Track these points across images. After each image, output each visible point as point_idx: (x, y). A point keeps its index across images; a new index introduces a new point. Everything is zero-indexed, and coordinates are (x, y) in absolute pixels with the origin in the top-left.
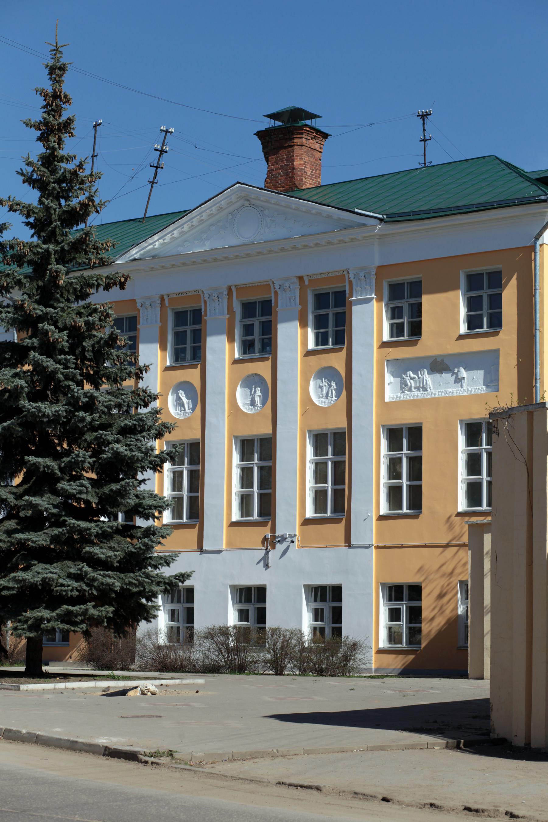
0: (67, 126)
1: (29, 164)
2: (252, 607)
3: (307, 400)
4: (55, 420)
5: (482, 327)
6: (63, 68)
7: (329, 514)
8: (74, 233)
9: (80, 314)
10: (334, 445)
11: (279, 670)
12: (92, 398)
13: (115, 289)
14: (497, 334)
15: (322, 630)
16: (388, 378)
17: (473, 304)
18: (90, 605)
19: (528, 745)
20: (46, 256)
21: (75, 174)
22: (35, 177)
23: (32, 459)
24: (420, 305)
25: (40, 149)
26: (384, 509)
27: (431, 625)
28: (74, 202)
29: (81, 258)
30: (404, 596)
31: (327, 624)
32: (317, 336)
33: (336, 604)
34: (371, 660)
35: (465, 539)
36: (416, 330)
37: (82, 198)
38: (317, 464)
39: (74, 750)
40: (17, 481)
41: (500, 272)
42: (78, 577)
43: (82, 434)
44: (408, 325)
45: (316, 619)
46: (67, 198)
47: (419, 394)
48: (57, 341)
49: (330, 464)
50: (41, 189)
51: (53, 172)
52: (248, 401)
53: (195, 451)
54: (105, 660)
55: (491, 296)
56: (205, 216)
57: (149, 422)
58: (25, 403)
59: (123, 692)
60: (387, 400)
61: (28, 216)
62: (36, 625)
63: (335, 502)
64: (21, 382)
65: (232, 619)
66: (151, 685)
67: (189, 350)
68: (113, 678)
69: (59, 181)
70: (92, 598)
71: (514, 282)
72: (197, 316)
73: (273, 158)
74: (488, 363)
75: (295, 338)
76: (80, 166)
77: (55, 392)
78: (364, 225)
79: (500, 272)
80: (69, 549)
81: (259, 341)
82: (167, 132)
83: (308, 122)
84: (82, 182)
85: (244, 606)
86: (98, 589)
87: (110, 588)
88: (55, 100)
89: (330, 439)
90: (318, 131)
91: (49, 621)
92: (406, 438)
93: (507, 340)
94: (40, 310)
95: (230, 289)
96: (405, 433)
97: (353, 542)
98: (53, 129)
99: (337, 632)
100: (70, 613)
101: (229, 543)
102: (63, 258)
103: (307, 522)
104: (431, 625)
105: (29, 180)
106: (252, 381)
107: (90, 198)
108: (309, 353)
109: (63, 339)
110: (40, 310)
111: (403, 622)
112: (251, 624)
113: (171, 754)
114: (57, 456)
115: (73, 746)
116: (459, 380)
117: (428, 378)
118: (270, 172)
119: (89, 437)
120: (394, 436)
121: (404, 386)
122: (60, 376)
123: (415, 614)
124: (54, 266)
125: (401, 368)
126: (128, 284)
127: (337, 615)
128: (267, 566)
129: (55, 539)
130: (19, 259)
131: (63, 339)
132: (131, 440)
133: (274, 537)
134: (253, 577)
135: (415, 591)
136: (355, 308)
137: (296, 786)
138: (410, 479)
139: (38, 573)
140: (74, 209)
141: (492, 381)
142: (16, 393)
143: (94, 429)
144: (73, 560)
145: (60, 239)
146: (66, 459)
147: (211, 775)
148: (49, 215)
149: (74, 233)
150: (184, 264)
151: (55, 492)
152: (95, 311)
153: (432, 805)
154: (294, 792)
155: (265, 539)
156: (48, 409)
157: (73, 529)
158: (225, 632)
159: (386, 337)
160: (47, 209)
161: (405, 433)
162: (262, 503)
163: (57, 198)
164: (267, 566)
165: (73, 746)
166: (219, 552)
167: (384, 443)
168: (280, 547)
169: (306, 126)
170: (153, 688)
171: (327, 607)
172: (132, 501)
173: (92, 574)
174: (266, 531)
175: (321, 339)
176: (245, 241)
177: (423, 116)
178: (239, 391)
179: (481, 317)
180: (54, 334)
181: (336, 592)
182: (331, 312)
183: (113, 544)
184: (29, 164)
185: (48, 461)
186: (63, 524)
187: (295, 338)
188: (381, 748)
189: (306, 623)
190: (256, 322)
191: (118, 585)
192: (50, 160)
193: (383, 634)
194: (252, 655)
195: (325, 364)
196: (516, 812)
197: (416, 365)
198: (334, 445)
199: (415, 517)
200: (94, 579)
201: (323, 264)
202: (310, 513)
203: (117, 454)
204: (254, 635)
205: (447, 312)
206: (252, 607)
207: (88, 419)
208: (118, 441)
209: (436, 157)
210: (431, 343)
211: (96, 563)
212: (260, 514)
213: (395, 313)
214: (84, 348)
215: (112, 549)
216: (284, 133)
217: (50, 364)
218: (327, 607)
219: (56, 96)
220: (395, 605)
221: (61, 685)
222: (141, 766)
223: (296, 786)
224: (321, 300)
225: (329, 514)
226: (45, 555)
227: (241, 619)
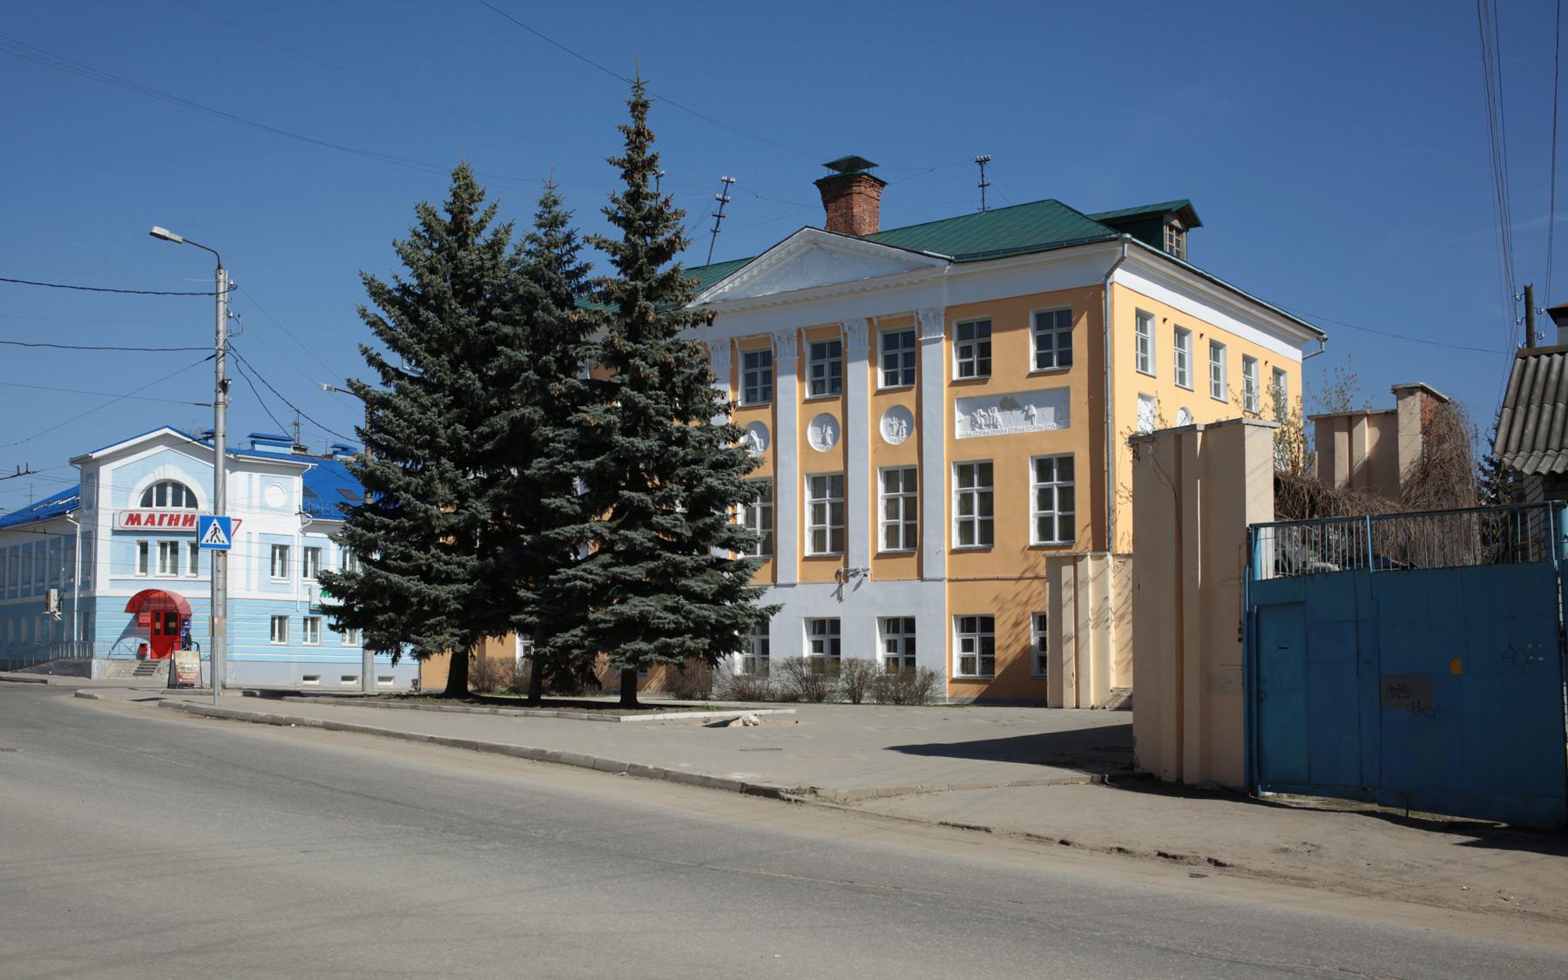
0: (650, 163)
1: (615, 201)
2: (826, 639)
3: (878, 438)
4: (648, 456)
5: (1051, 364)
6: (645, 105)
7: (901, 548)
8: (663, 269)
9: (669, 350)
10: (905, 482)
11: (856, 698)
12: (685, 433)
13: (703, 326)
14: (1067, 371)
15: (896, 660)
16: (958, 415)
17: (1042, 343)
18: (687, 636)
19: (1180, 780)
20: (633, 293)
21: (661, 211)
22: (620, 214)
23: (626, 493)
24: (989, 344)
25: (623, 187)
26: (956, 543)
27: (1005, 654)
28: (660, 239)
29: (667, 295)
30: (978, 627)
31: (900, 655)
32: (886, 375)
33: (909, 636)
34: (945, 689)
35: (1044, 573)
36: (986, 369)
37: (669, 234)
38: (815, 506)
39: (708, 786)
40: (607, 516)
41: (1069, 311)
42: (674, 610)
43: (674, 468)
44: (977, 362)
45: (889, 650)
46: (653, 236)
47: (989, 432)
48: (648, 377)
49: (828, 507)
50: (625, 227)
51: (639, 209)
52: (819, 439)
53: (767, 491)
54: (686, 691)
55: (1060, 335)
56: (774, 260)
57: (740, 457)
58: (618, 438)
59: (725, 724)
61: (614, 254)
62: (635, 657)
63: (908, 536)
64: (614, 418)
65: (807, 651)
66: (750, 715)
67: (761, 390)
68: (708, 708)
69: (644, 219)
70: (688, 630)
71: (1084, 320)
72: (767, 358)
73: (832, 206)
74: (1059, 401)
75: (865, 377)
76: (666, 202)
77: (645, 429)
79: (1069, 311)
80: (663, 582)
81: (829, 377)
84: (668, 220)
85: (818, 638)
86: (694, 621)
87: (706, 620)
88: (638, 138)
89: (901, 476)
90: (875, 179)
91: (646, 653)
92: (977, 474)
93: (1077, 378)
94: (629, 346)
95: (799, 331)
96: (1055, 463)
97: (926, 575)
98: (636, 167)
99: (911, 662)
100: (667, 645)
101: (802, 577)
102: (651, 295)
103: (879, 556)
104: (1005, 654)
105: (614, 218)
106: (823, 420)
107: (677, 235)
108: (879, 393)
109: (654, 375)
110: (629, 346)
111: (976, 653)
112: (825, 654)
113: (814, 791)
114: (648, 491)
115: (705, 783)
116: (1029, 417)
117: (998, 415)
118: (829, 220)
119: (681, 471)
120: (965, 472)
121: (974, 423)
122: (652, 411)
123: (988, 646)
124: (642, 302)
125: (970, 405)
126: (715, 322)
127: (910, 646)
128: (840, 599)
129: (650, 573)
130: (606, 297)
131: (654, 375)
132: (723, 474)
133: (847, 571)
134: (827, 611)
135: (988, 623)
136: (924, 348)
137: (962, 827)
138: (833, 522)
139: (635, 606)
140: (660, 247)
141: (1063, 418)
142: (608, 429)
143: (686, 463)
144: (669, 593)
145: (646, 276)
146: (659, 494)
147: (864, 814)
148: (636, 253)
149: (663, 269)
150: (754, 308)
151: (651, 526)
152: (684, 347)
153: (1120, 850)
154: (966, 833)
155: (838, 573)
156: (640, 443)
157: (668, 562)
158: (800, 662)
159: (956, 376)
160: (634, 245)
161: (1055, 463)
162: (834, 538)
163: (643, 235)
164: (840, 599)
165: (705, 783)
166: (793, 585)
167: (955, 479)
168: (853, 581)
170: (755, 719)
171: (900, 638)
172: (725, 535)
173: (688, 606)
174: (839, 565)
175: (891, 379)
176: (814, 284)
177: (981, 162)
178: (810, 430)
179: (1051, 355)
180: (646, 370)
181: (910, 624)
182: (900, 353)
183: (706, 577)
184: (615, 201)
185: (642, 496)
186: (659, 557)
187: (865, 377)
188: (1026, 784)
189: (880, 653)
190: (826, 363)
191: (714, 616)
192: (635, 197)
193: (957, 664)
194: (828, 685)
195: (895, 403)
196: (1222, 860)
197: (986, 403)
198: (905, 482)
199: (988, 550)
200: (690, 612)
201: (891, 306)
202: (882, 548)
203: (710, 488)
204: (828, 667)
205: (1016, 351)
206: (826, 639)
207: (681, 453)
208: (710, 475)
209: (996, 201)
210: (1003, 378)
211: (698, 598)
212: (833, 549)
213: (964, 352)
214: (674, 385)
215: (706, 582)
216: (842, 183)
217: (641, 399)
218: (900, 638)
219: (639, 133)
220: (968, 636)
221: (660, 716)
222: (783, 804)
223: (962, 827)
224: (890, 341)
225: (901, 548)
226: (639, 588)
227: (815, 650)
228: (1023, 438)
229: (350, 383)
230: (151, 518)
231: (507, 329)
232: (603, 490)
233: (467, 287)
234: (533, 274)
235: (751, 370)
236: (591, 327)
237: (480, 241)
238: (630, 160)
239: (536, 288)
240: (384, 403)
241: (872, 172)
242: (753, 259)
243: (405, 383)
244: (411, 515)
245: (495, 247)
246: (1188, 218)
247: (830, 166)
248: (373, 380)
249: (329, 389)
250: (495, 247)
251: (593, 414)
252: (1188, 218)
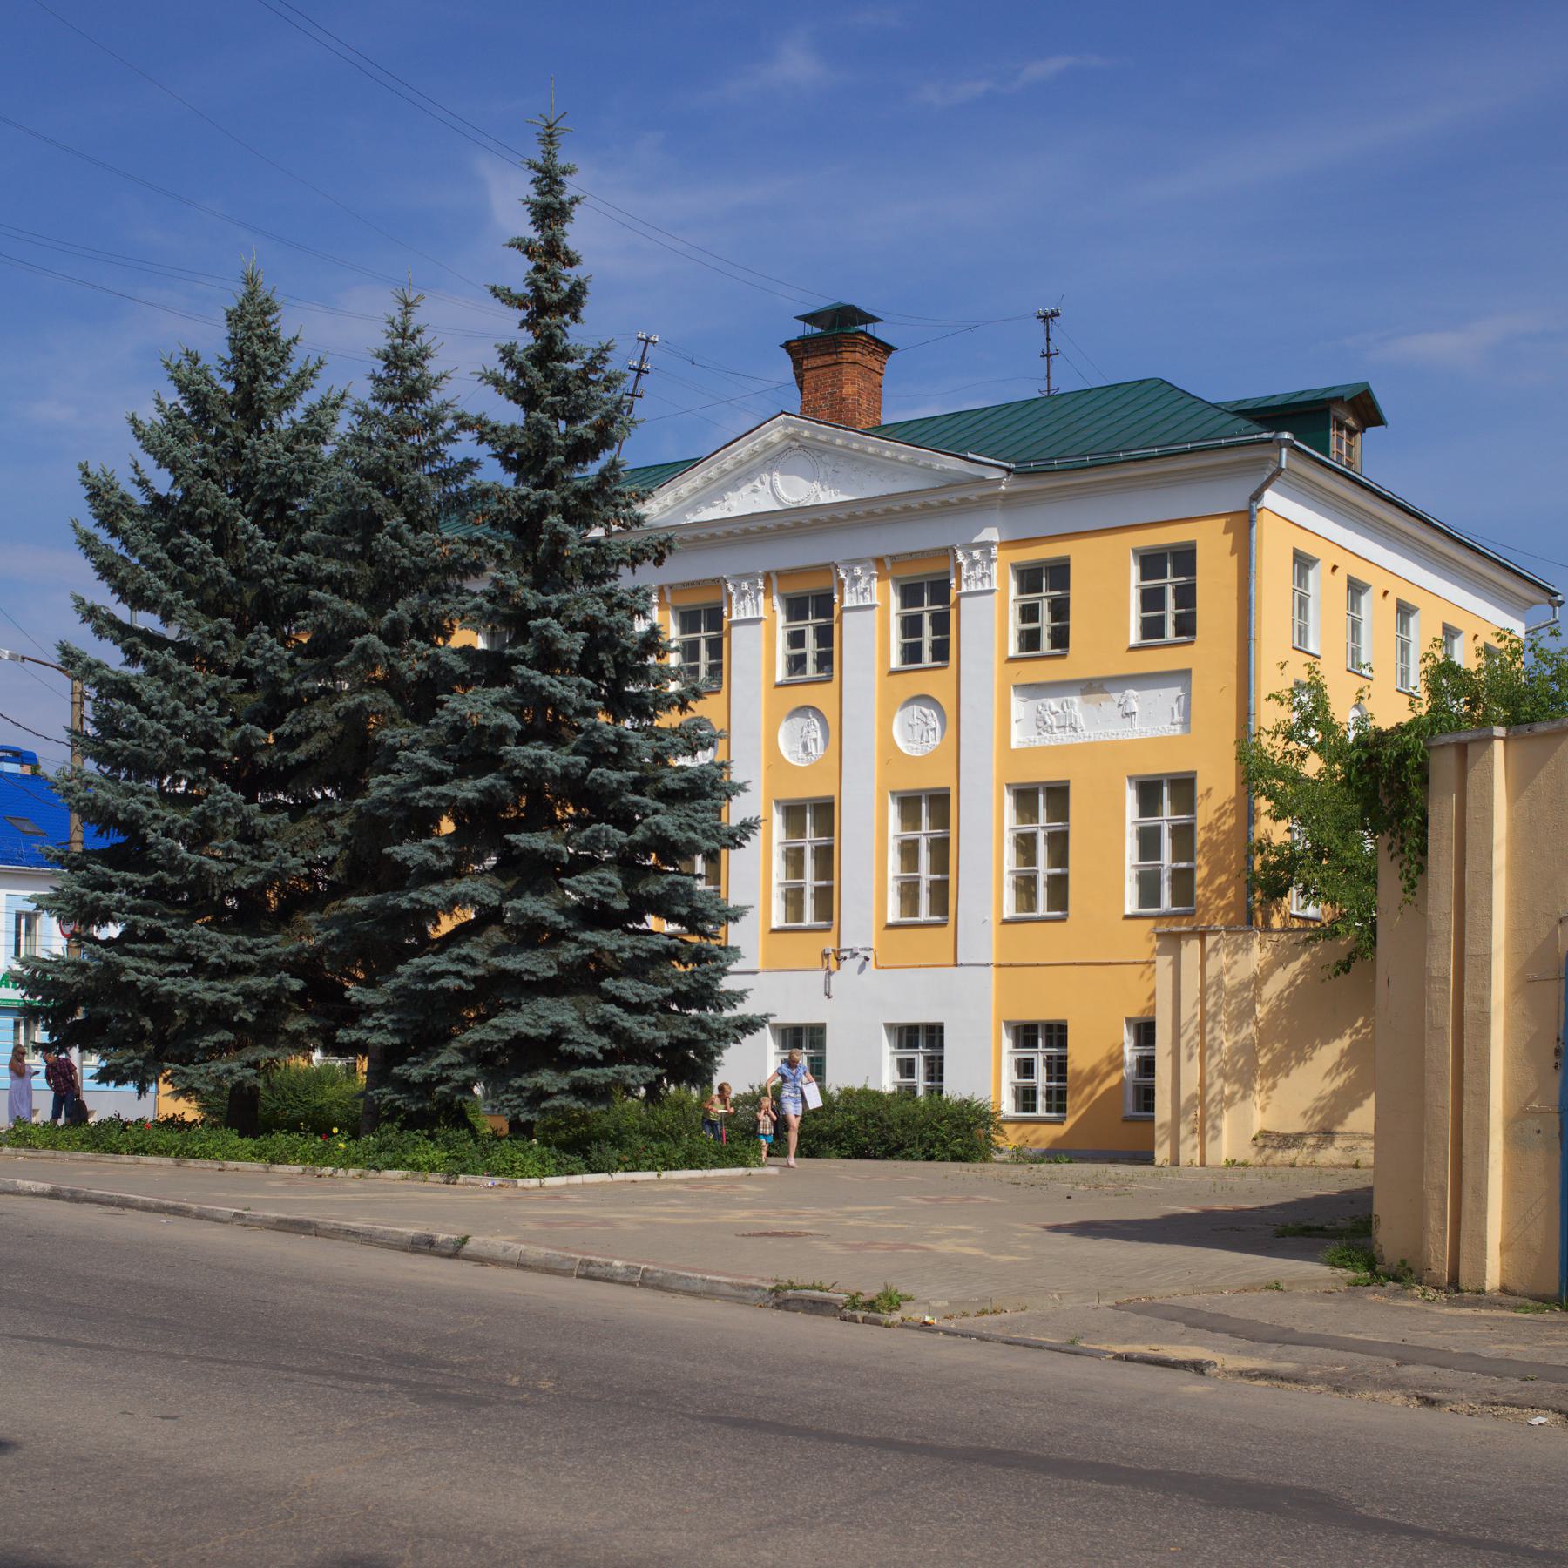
3: (888, 746)
10: (929, 807)
20: (543, 509)
36: (1061, 639)
47: (1065, 738)
60: (1014, 745)
63: (932, 893)
78: (982, 479)
80: (582, 979)
82: (647, 341)
83: (862, 328)
90: (878, 341)
92: (1044, 798)
109: (573, 643)
120: (1025, 797)
132: (682, 809)
168: (850, 965)
169: (862, 333)
174: (827, 942)
177: (1047, 318)
192: (548, 352)
198: (929, 807)
202: (893, 916)
209: (1067, 380)
210: (1082, 659)
220: (907, 1053)
228: (1116, 748)
229: (65, 651)
231: (331, 566)
232: (482, 823)
233: (274, 502)
234: (380, 476)
236: (477, 569)
237: (283, 424)
238: (539, 298)
239: (380, 502)
240: (125, 690)
241: (871, 329)
242: (693, 463)
243: (167, 655)
244: (177, 868)
245: (313, 431)
246: (1365, 410)
247: (807, 319)
249: (12, 658)
250: (313, 431)
251: (475, 705)
252: (1365, 410)
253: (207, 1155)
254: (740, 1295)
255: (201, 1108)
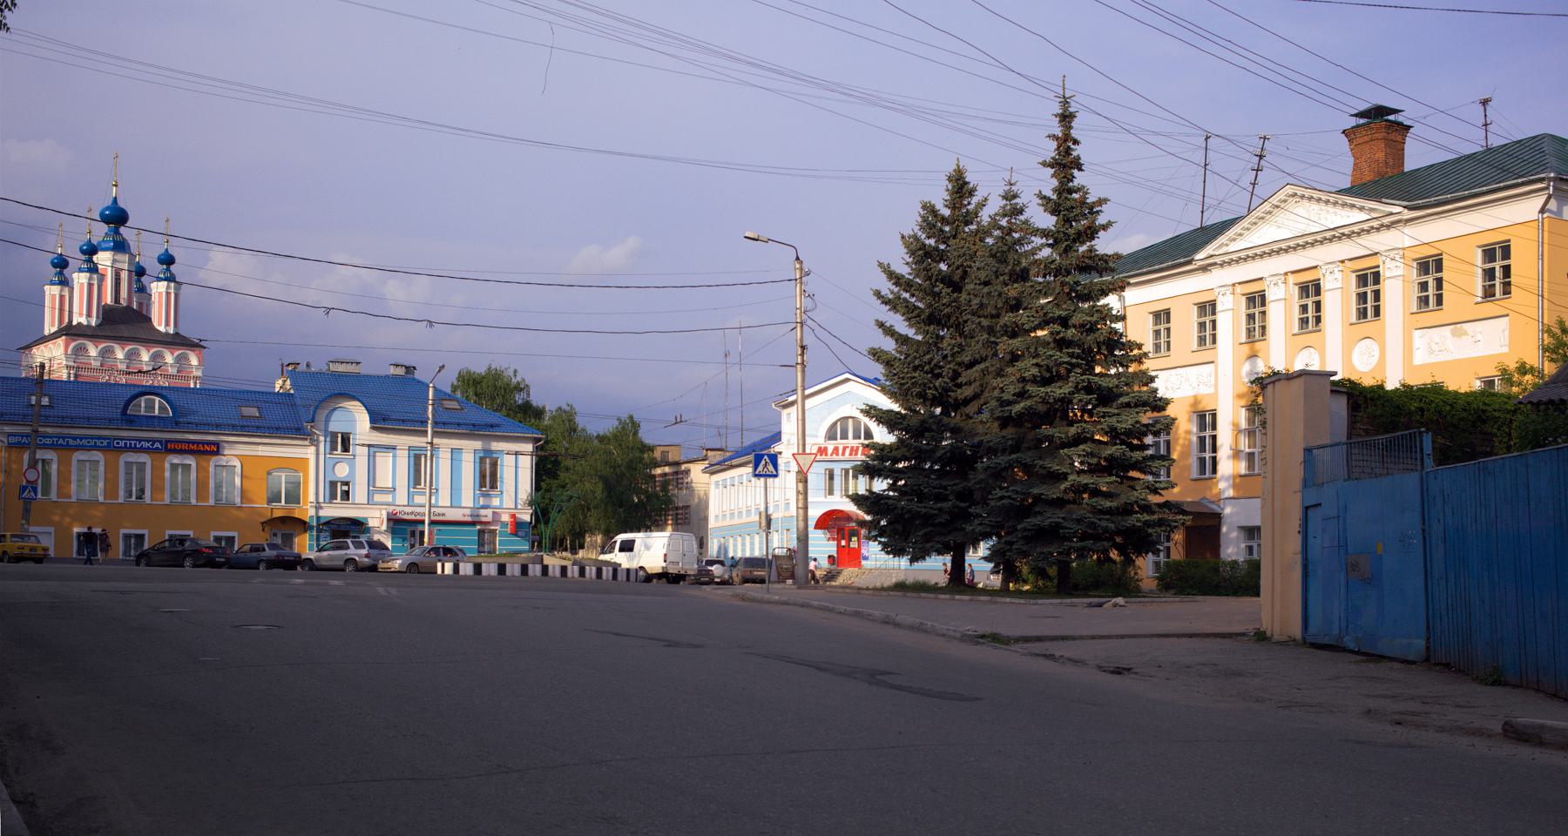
6: (1072, 116)
88: (1066, 143)
177: (1485, 102)
192: (1065, 189)
209: (1495, 142)
230: (836, 450)
235: (1362, 290)
248: (889, 345)
253: (735, 563)
254: (967, 638)
255: (940, 553)
